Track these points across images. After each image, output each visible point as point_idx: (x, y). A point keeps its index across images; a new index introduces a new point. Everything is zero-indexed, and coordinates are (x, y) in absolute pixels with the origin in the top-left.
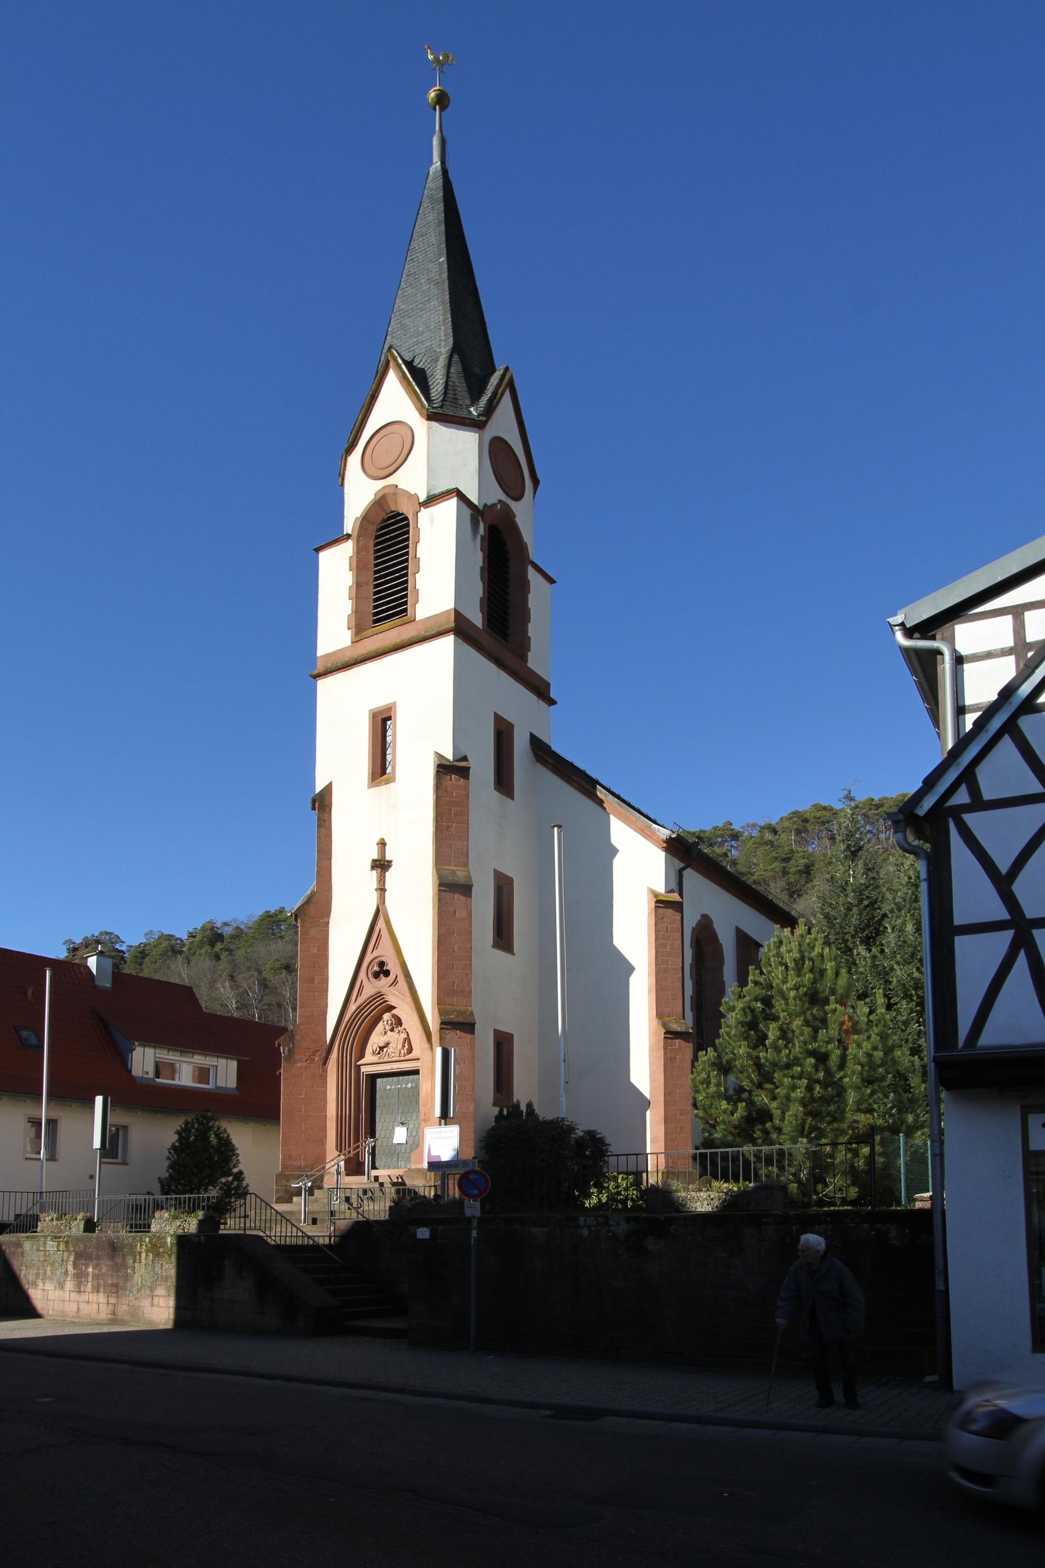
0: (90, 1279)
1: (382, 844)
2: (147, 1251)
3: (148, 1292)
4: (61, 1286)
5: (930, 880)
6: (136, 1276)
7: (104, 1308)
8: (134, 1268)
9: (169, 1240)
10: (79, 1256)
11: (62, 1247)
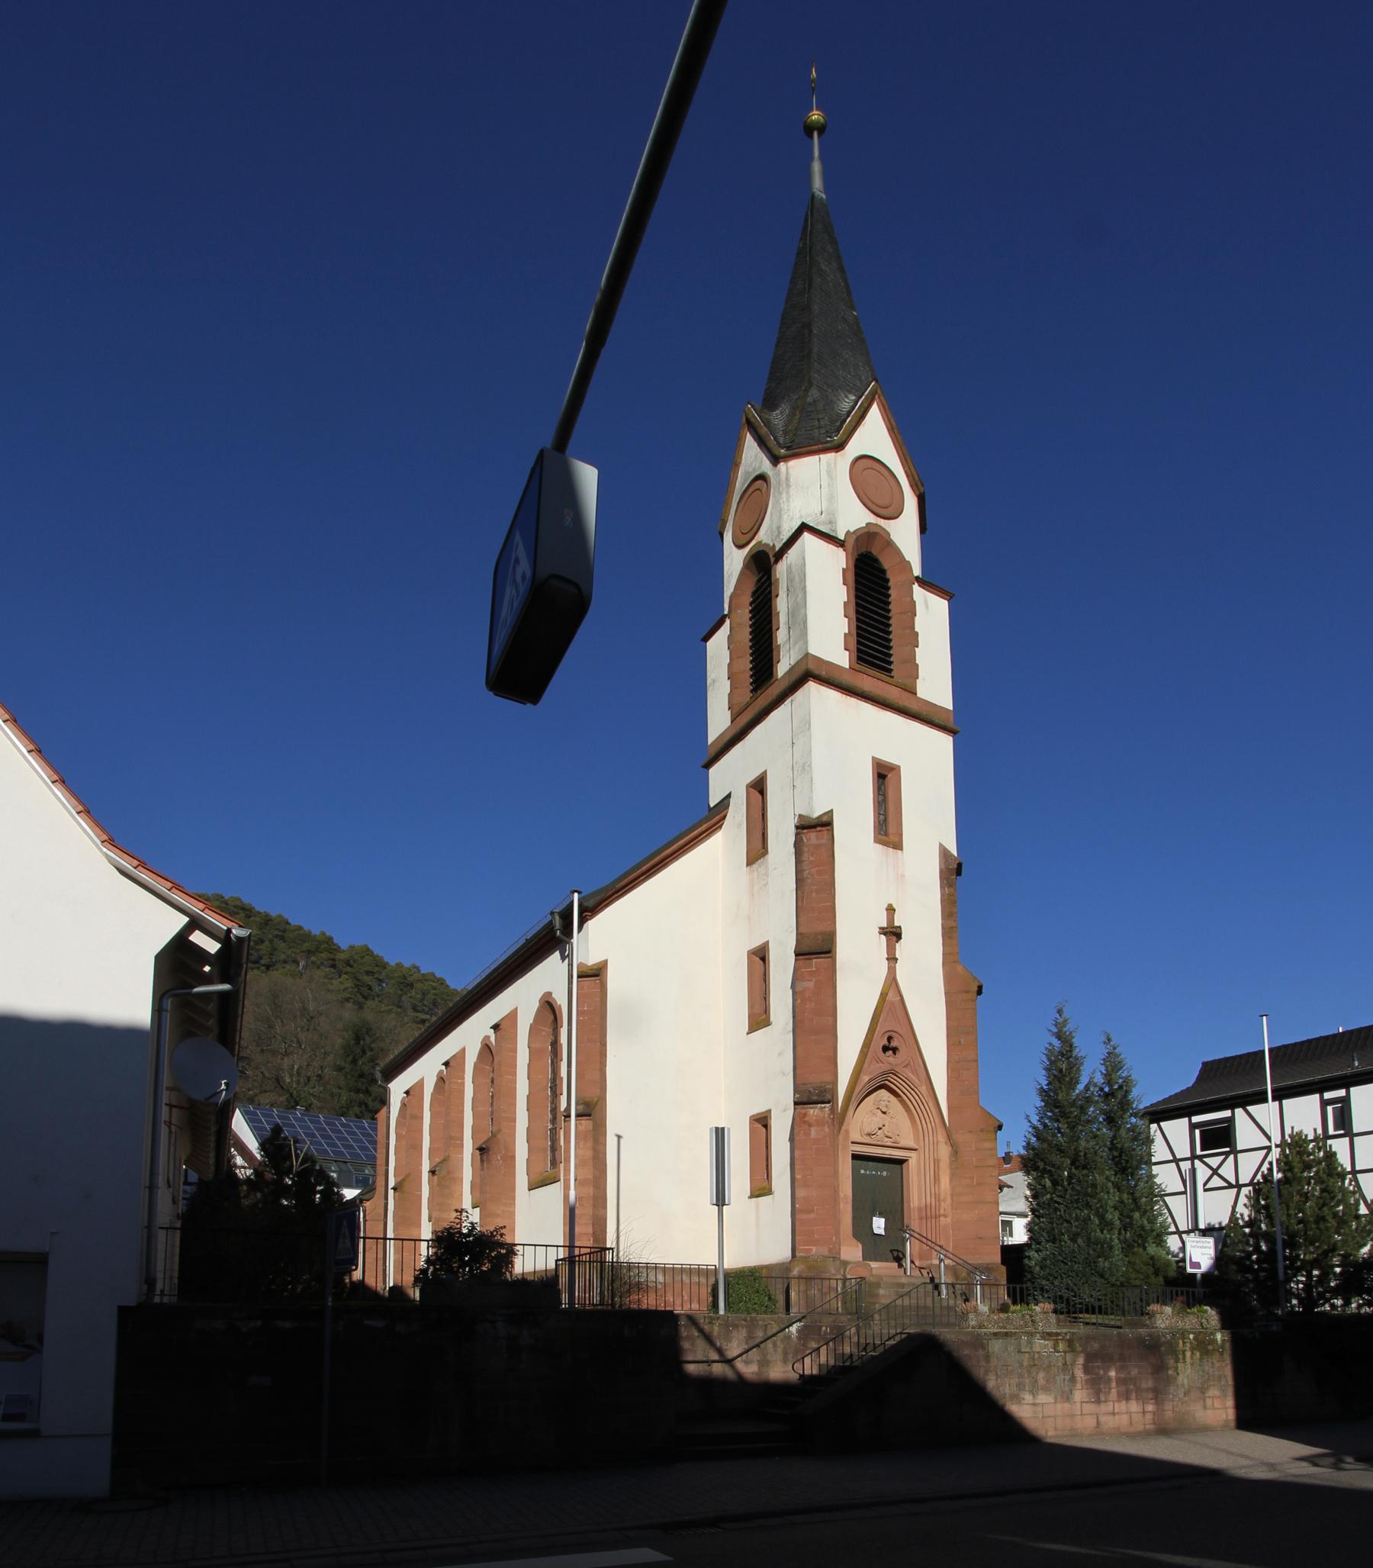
0: (1114, 1384)
1: (891, 910)
2: (1192, 1350)
4: (1067, 1397)
6: (1180, 1378)
7: (1137, 1418)
8: (1176, 1369)
9: (1219, 1336)
10: (1090, 1358)
11: (1061, 1346)
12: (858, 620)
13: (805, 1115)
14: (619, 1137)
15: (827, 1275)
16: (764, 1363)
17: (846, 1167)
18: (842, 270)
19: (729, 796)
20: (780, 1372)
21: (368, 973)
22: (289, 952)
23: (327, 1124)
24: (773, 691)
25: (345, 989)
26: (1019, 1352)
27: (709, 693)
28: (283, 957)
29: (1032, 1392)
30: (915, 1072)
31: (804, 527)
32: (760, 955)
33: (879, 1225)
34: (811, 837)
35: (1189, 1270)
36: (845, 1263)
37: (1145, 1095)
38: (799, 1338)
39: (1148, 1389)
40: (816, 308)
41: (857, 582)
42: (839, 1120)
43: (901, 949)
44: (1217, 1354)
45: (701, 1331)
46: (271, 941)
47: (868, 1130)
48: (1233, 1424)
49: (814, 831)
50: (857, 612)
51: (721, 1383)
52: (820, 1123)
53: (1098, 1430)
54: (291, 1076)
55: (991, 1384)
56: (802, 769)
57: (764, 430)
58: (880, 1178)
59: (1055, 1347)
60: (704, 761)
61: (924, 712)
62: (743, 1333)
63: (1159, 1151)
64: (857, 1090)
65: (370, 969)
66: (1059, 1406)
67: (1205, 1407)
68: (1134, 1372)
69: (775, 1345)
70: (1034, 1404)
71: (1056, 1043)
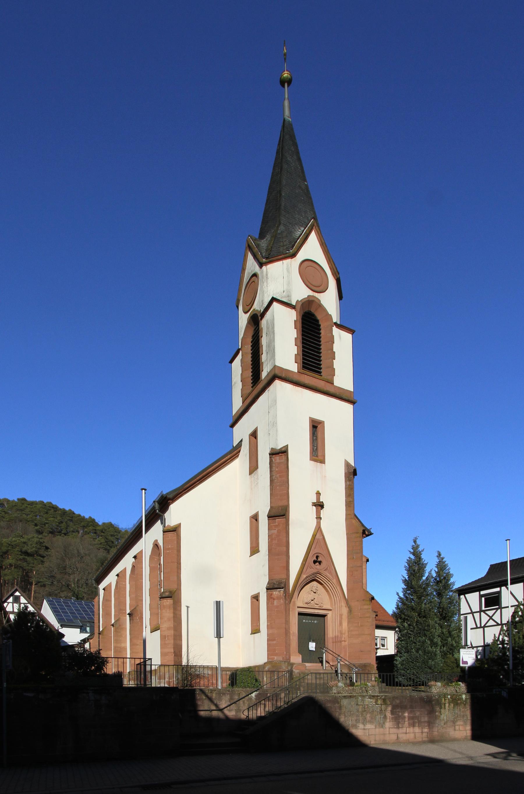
0: (407, 719)
1: (318, 494)
3: (451, 724)
4: (382, 726)
5: (479, 591)
6: (442, 716)
8: (440, 712)
9: (464, 696)
10: (394, 707)
12: (303, 347)
13: (272, 594)
14: (188, 607)
15: (281, 670)
16: (238, 710)
17: (294, 620)
18: (299, 159)
19: (241, 441)
20: (244, 713)
21: (112, 535)
22: (74, 527)
23: (64, 602)
24: (260, 386)
25: (101, 543)
26: (357, 705)
27: (233, 387)
28: (72, 529)
29: (363, 723)
30: (330, 573)
31: (273, 300)
32: (255, 518)
33: (312, 646)
34: (277, 459)
35: (461, 665)
36: (292, 664)
37: (459, 580)
38: (256, 699)
39: (425, 722)
40: (284, 182)
41: (303, 327)
42: (289, 597)
43: (323, 513)
44: (463, 705)
45: (207, 696)
46: (66, 522)
47: (306, 601)
48: (469, 738)
49: (280, 455)
50: (303, 343)
51: (217, 720)
52: (279, 598)
53: (398, 741)
54: (74, 583)
55: (342, 719)
56: (274, 424)
57: (256, 250)
58: (313, 624)
59: (376, 702)
60: (231, 422)
61: (338, 393)
62: (228, 697)
63: (464, 609)
64: (300, 582)
65: (112, 533)
66: (377, 730)
67: (455, 730)
68: (418, 714)
69: (244, 702)
70: (364, 729)
71: (413, 557)
